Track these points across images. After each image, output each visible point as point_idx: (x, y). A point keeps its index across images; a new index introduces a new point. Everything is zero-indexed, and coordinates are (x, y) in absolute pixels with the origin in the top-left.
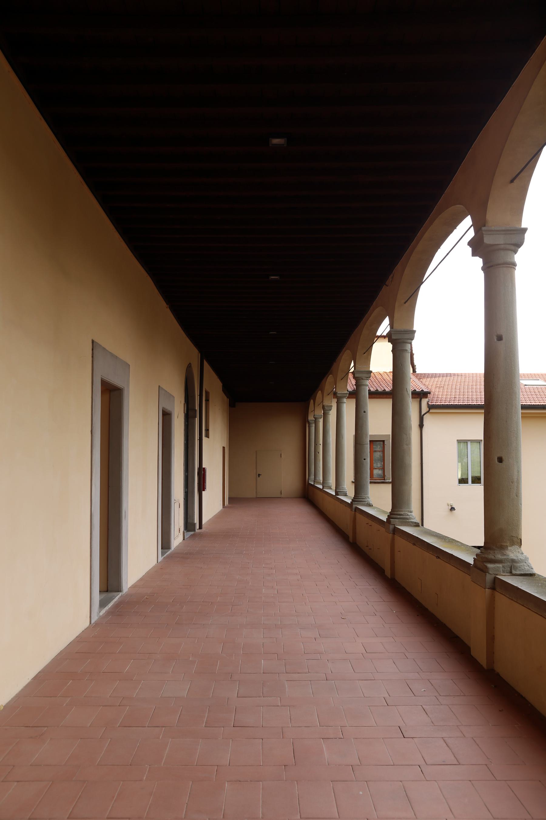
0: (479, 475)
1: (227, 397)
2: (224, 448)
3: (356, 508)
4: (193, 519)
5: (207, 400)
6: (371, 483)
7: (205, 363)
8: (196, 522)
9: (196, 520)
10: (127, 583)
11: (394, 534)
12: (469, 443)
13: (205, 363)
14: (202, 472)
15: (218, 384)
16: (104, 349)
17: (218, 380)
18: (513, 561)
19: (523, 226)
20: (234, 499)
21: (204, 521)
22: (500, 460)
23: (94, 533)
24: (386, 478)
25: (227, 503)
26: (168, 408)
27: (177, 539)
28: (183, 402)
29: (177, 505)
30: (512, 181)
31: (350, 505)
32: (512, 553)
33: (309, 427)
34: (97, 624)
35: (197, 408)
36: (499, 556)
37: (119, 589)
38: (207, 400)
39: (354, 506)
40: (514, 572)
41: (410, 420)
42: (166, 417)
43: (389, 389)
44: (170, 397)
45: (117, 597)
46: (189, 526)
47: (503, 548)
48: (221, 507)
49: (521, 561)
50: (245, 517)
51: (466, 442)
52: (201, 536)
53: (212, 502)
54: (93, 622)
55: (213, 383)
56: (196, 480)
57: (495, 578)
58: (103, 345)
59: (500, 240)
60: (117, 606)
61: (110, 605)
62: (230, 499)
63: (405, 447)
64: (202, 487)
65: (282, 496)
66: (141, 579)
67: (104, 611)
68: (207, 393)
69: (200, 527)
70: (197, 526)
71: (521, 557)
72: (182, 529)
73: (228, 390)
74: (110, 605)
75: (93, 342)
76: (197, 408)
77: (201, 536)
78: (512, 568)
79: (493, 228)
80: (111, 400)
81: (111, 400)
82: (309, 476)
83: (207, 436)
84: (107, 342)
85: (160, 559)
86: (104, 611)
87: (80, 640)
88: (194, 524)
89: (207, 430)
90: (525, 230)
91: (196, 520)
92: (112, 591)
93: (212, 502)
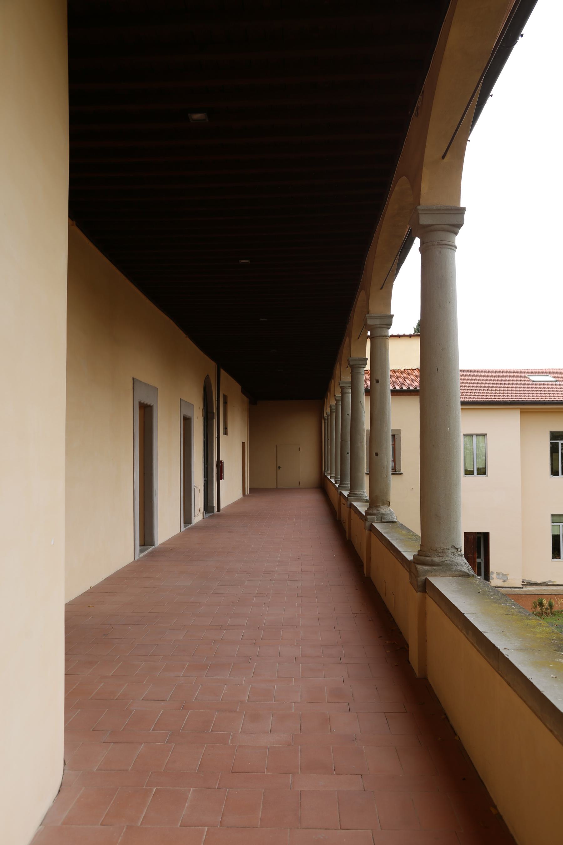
0: (484, 467)
1: (247, 397)
2: (244, 443)
3: (341, 492)
4: (213, 503)
5: (225, 403)
6: (393, 474)
7: (222, 371)
8: (215, 505)
9: (215, 504)
10: (158, 540)
11: (350, 508)
12: (475, 437)
13: (222, 371)
14: (220, 465)
15: (236, 387)
16: (141, 381)
17: (237, 383)
18: (383, 514)
19: (391, 314)
20: (255, 488)
21: (222, 507)
22: (377, 454)
23: (136, 502)
24: (396, 469)
25: (247, 492)
26: (188, 414)
27: (197, 517)
28: (202, 407)
29: (197, 490)
30: (381, 288)
31: (337, 489)
32: (383, 510)
33: (325, 422)
34: (138, 560)
35: (215, 411)
36: (375, 512)
37: (152, 544)
38: (225, 403)
39: (339, 491)
40: (383, 521)
41: (363, 424)
42: (187, 422)
43: (414, 383)
44: (190, 405)
45: (151, 549)
46: (208, 508)
47: (377, 507)
48: (241, 496)
49: (388, 514)
50: (261, 503)
51: (471, 435)
52: (219, 516)
53: (231, 490)
54: (136, 559)
55: (230, 386)
56: (214, 471)
57: (372, 525)
58: (140, 379)
59: (377, 322)
60: (151, 553)
61: (147, 552)
62: (250, 489)
63: (359, 444)
64: (220, 476)
65: (301, 486)
66: (168, 541)
67: (142, 555)
68: (225, 397)
69: (219, 510)
70: (216, 509)
71: (388, 512)
72: (202, 509)
73: (246, 391)
74: (147, 552)
75: (133, 378)
76: (215, 411)
77: (219, 516)
78: (382, 519)
79: (373, 315)
80: (146, 416)
81: (146, 416)
82: (325, 468)
83: (226, 433)
84: (144, 377)
85: (183, 529)
86: (142, 555)
87: (128, 566)
88: (213, 508)
89: (226, 429)
90: (392, 316)
91: (215, 504)
92: (147, 545)
93: (231, 490)
